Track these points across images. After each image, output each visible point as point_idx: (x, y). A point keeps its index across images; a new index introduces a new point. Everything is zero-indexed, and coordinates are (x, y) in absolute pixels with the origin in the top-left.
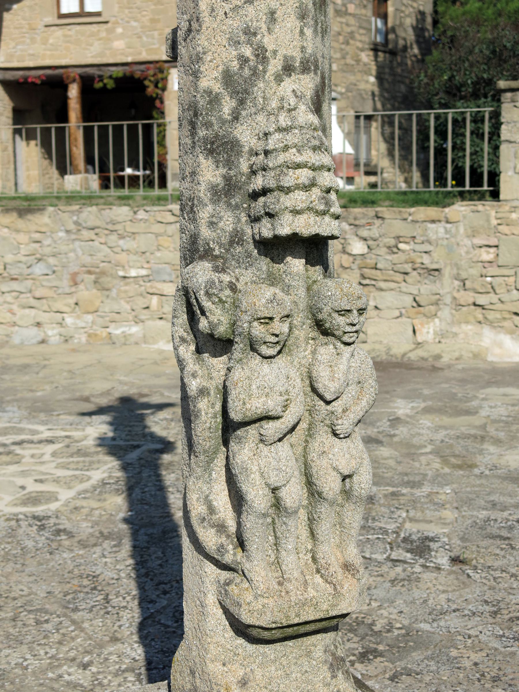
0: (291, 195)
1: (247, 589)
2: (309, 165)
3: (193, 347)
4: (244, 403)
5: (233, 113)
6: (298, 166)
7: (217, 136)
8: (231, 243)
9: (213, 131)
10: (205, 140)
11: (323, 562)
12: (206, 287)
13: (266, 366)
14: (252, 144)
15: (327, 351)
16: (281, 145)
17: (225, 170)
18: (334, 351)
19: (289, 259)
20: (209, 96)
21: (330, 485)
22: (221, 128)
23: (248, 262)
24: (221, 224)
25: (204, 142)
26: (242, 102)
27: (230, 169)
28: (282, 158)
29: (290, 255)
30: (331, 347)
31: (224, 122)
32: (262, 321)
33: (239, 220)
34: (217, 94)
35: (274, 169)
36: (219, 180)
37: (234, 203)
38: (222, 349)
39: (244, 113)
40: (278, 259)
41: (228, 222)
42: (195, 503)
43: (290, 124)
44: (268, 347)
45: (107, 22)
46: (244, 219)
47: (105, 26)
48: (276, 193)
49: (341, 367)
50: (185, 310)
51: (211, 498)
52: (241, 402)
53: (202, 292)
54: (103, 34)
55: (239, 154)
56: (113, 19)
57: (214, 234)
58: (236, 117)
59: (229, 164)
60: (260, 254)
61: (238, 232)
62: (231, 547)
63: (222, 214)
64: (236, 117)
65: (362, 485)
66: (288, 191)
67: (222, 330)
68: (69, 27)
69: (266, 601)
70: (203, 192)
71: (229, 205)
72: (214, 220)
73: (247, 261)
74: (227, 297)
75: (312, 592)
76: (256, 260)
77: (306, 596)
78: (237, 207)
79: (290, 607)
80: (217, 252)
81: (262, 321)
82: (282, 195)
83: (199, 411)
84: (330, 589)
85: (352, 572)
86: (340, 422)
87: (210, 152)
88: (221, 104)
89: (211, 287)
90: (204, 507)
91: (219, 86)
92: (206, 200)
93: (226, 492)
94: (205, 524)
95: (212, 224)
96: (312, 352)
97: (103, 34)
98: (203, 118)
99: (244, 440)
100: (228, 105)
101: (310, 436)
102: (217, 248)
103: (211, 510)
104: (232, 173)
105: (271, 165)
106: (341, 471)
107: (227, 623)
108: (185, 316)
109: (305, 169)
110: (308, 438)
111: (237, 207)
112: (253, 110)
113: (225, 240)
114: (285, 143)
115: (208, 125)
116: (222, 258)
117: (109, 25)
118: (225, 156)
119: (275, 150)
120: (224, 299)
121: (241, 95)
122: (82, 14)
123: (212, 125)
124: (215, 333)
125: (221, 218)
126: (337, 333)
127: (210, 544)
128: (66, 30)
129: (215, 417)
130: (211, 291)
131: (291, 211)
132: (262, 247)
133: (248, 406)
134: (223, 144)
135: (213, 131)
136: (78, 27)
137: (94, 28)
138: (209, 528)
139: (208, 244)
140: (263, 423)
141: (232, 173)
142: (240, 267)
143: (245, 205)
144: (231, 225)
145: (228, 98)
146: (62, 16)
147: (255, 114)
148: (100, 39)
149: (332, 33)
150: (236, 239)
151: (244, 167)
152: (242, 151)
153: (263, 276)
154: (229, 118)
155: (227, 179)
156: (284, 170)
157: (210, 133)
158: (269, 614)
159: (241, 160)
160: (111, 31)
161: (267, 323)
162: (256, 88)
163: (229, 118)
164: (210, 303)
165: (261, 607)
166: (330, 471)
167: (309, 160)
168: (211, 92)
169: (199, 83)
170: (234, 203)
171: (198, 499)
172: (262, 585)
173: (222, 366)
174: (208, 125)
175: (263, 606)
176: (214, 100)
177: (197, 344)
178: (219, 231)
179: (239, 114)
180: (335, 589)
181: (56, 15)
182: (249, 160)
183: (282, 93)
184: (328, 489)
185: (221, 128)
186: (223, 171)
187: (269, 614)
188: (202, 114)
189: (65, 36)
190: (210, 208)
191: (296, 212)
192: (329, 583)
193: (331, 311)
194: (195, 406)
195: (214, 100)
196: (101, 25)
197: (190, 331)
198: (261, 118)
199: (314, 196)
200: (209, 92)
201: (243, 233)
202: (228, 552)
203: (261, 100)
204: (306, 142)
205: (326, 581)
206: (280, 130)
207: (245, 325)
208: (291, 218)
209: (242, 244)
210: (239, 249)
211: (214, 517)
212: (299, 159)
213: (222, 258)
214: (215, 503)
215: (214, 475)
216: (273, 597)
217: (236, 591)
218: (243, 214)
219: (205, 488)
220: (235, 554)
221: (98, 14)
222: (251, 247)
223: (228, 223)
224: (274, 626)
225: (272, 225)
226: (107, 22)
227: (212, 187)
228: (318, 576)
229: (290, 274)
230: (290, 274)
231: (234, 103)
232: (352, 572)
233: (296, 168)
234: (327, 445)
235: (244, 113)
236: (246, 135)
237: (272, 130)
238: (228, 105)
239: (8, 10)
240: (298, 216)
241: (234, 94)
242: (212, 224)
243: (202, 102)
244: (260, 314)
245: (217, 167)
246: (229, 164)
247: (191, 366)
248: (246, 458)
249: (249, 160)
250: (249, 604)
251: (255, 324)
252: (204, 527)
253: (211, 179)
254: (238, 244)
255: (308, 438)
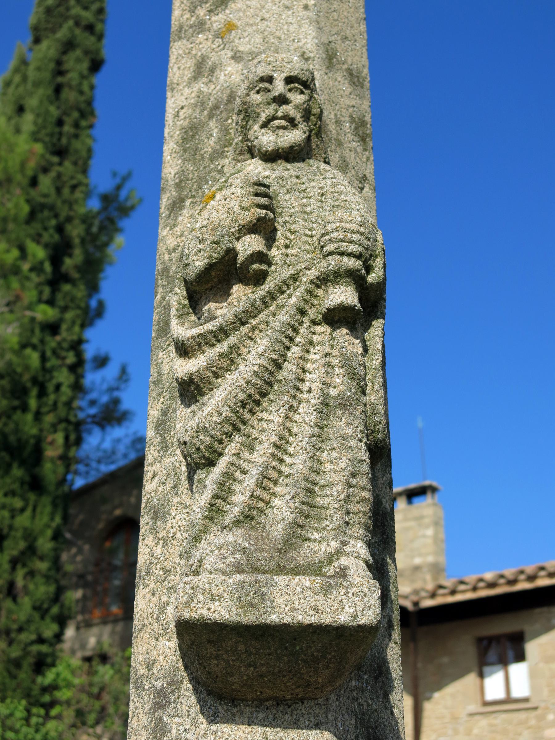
45: (536, 708)
47: (533, 714)
54: (533, 722)
56: (542, 705)
68: (494, 715)
97: (533, 722)
117: (539, 712)
122: (509, 700)
128: (491, 720)
129: (137, 605)
136: (504, 716)
137: (522, 716)
146: (486, 704)
148: (529, 728)
149: (77, 241)
160: (542, 718)
169: (96, 340)
181: (479, 702)
189: (491, 725)
196: (530, 711)
221: (526, 700)
226: (536, 708)
239: (429, 699)
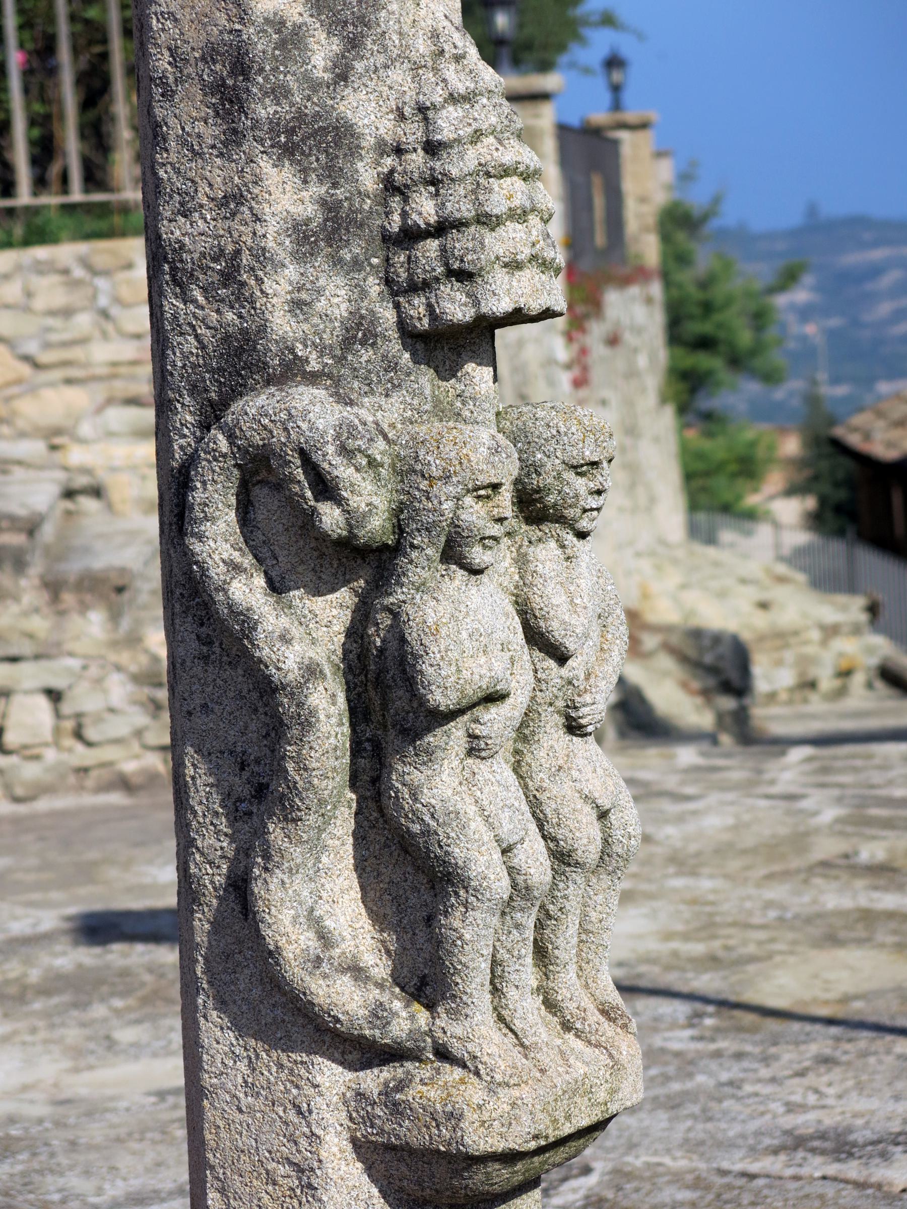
0: (501, 230)
1: (462, 1081)
2: (521, 168)
3: (260, 581)
4: (459, 671)
5: (335, 66)
6: (506, 172)
7: (300, 117)
8: (348, 343)
9: (292, 105)
10: (274, 126)
11: (572, 1006)
12: (338, 436)
13: (474, 590)
14: (382, 131)
15: (546, 555)
16: (469, 130)
17: (323, 189)
18: (559, 552)
19: (470, 367)
20: (278, 32)
21: (585, 836)
22: (309, 99)
23: (390, 381)
24: (321, 305)
25: (271, 130)
26: (354, 43)
27: (335, 185)
28: (472, 157)
29: (471, 359)
30: (553, 544)
31: (315, 86)
32: (482, 492)
33: (364, 294)
34: (297, 28)
35: (462, 179)
36: (310, 210)
37: (348, 257)
38: (335, 575)
39: (359, 66)
40: (448, 370)
41: (336, 298)
42: (290, 929)
43: (472, 86)
44: (485, 547)
46: (374, 286)
48: (473, 228)
49: (582, 582)
50: (233, 500)
51: (317, 913)
52: (453, 668)
53: (330, 449)
55: (354, 151)
57: (305, 327)
58: (342, 74)
59: (332, 174)
60: (416, 362)
61: (362, 317)
62: (397, 1005)
63: (322, 282)
64: (342, 74)
65: (630, 829)
66: (487, 221)
67: (377, 527)
69: (516, 1092)
70: (273, 236)
71: (336, 261)
72: (304, 296)
73: (390, 378)
74: (382, 453)
75: (580, 1069)
76: (408, 374)
77: (575, 1075)
78: (356, 265)
79: (556, 1100)
80: (314, 365)
81: (482, 492)
82: (485, 231)
83: (313, 713)
84: (604, 1059)
85: (620, 1022)
86: (588, 698)
87: (288, 151)
88: (307, 49)
89: (351, 436)
90: (311, 934)
91: (300, 9)
92: (282, 255)
93: (356, 893)
94: (325, 967)
95: (298, 306)
96: (516, 561)
98: (266, 79)
99: (439, 754)
100: (322, 51)
101: (525, 739)
102: (314, 356)
103: (325, 938)
104: (340, 193)
105: (455, 172)
106: (599, 802)
107: (375, 1191)
108: (232, 516)
109: (515, 178)
110: (520, 746)
111: (356, 265)
112: (381, 59)
113: (332, 336)
114: (475, 126)
115: (279, 93)
116: (330, 376)
118: (322, 157)
119: (458, 140)
120: (378, 457)
121: (351, 28)
123: (287, 93)
124: (361, 533)
125: (319, 292)
126: (570, 513)
127: (352, 1007)
129: (341, 724)
130: (351, 444)
131: (506, 265)
132: (420, 346)
133: (466, 674)
134: (316, 132)
135: (292, 105)
138: (337, 976)
139: (292, 350)
140: (478, 711)
141: (340, 193)
142: (372, 392)
143: (375, 261)
144: (344, 306)
145: (322, 36)
147: (386, 67)
150: (359, 331)
151: (367, 176)
152: (359, 147)
153: (427, 407)
154: (327, 76)
155: (329, 206)
156: (482, 181)
157: (285, 110)
158: (525, 1118)
159: (360, 165)
161: (488, 497)
162: (383, 13)
163: (327, 76)
164: (352, 470)
165: (507, 1108)
166: (580, 804)
167: (519, 159)
168: (283, 23)
170: (348, 257)
171: (295, 920)
172: (500, 1062)
173: (335, 612)
174: (279, 93)
175: (513, 1105)
176: (291, 40)
177: (266, 573)
178: (316, 320)
179: (349, 67)
180: (611, 1056)
182: (378, 164)
183: (430, 22)
184: (585, 841)
185: (309, 99)
186: (317, 189)
187: (525, 1118)
188: (261, 70)
190: (291, 271)
191: (514, 266)
192: (596, 1046)
193: (561, 467)
194: (300, 705)
195: (291, 40)
197: (244, 546)
198: (398, 76)
199: (534, 233)
200: (277, 23)
201: (374, 319)
202: (395, 1014)
203: (395, 37)
204: (506, 122)
205: (589, 1042)
206: (453, 99)
207: (448, 506)
208: (507, 278)
209: (373, 345)
210: (366, 354)
211: (336, 952)
212: (507, 157)
213: (330, 376)
214: (329, 923)
215: (324, 859)
216: (526, 1083)
217: (433, 1093)
218: (371, 280)
219: (305, 893)
220: (412, 1017)
222: (395, 346)
223: (335, 300)
224: (533, 1145)
225: (468, 295)
227: (296, 226)
228: (570, 1036)
229: (474, 399)
230: (474, 399)
231: (336, 46)
232: (620, 1022)
233: (502, 177)
234: (561, 753)
235: (359, 66)
236: (367, 111)
237: (438, 100)
238: (322, 51)
240: (518, 274)
241: (335, 25)
242: (298, 306)
243: (262, 45)
244: (481, 478)
245: (305, 182)
246: (332, 174)
247: (272, 619)
248: (450, 792)
249: (378, 164)
250: (480, 1107)
251: (469, 500)
252: (325, 976)
253: (292, 209)
254: (363, 343)
255: (520, 746)
